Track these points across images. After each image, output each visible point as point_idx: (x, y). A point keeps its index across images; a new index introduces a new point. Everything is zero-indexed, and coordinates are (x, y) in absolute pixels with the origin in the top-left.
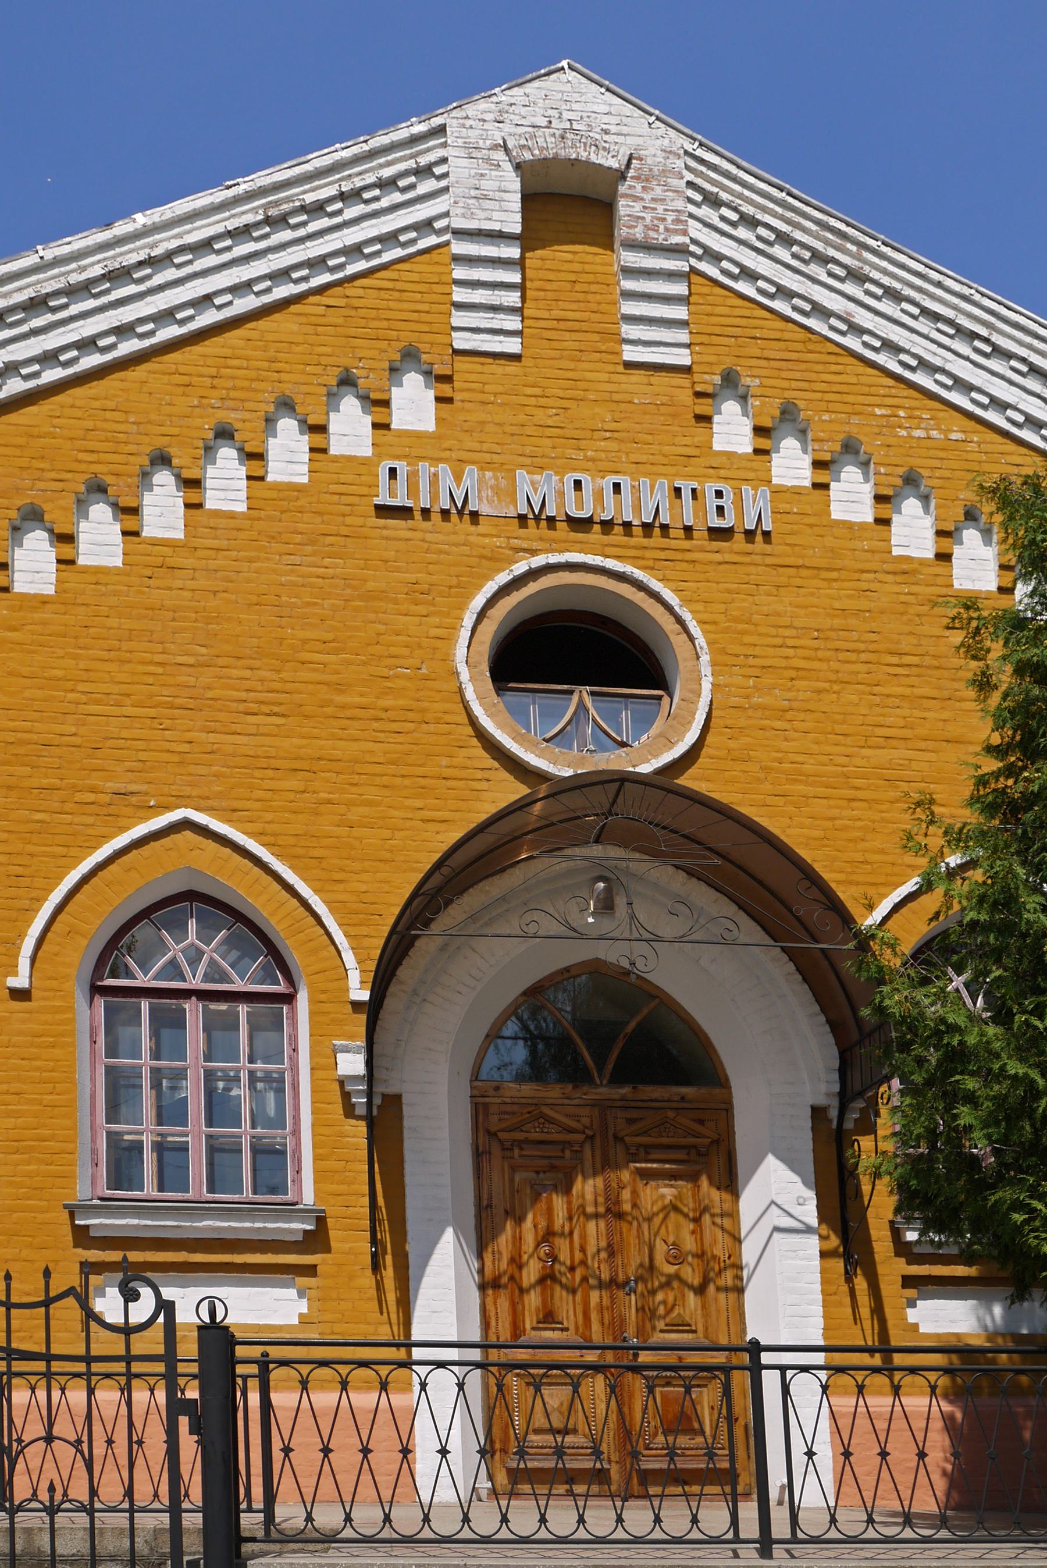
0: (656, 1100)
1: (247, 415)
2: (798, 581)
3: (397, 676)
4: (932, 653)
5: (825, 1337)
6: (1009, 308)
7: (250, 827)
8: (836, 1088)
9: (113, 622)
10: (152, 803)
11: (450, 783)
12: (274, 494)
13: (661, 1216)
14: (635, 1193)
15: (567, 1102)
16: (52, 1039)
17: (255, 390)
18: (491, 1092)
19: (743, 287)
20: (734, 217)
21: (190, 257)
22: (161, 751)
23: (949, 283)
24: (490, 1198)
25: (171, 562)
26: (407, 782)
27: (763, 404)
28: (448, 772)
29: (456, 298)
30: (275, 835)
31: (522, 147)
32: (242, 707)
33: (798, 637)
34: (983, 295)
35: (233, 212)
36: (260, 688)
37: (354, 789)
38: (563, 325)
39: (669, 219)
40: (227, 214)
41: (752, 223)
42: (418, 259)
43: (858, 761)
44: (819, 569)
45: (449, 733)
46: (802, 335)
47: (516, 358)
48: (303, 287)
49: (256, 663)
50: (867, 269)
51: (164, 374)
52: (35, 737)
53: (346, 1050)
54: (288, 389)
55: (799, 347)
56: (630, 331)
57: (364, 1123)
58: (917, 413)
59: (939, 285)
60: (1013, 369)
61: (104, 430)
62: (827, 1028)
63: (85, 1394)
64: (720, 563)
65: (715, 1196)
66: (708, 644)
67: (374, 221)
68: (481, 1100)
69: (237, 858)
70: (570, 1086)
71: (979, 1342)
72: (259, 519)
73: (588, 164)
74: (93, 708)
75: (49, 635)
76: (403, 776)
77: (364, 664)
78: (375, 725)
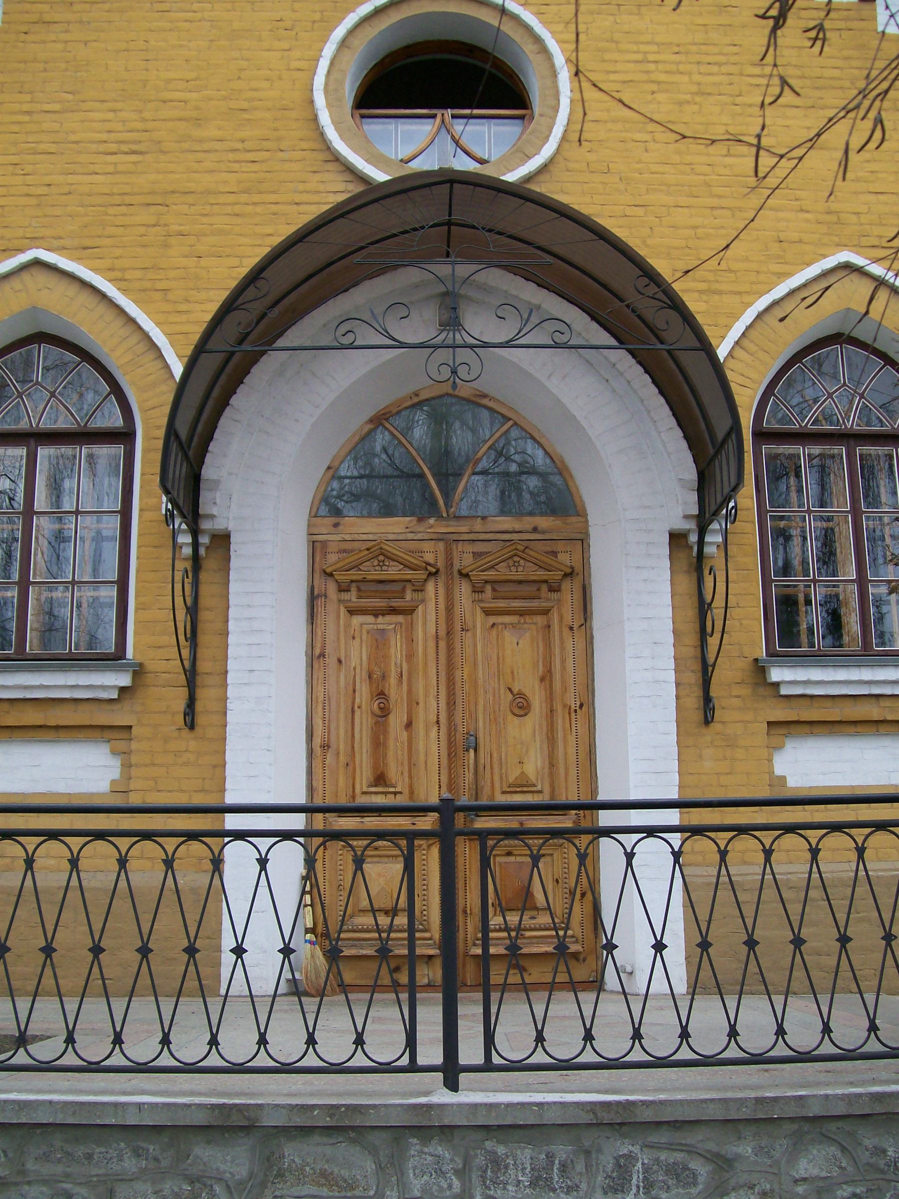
4: (794, 63)
7: (98, 263)
8: (695, 512)
15: (410, 536)
24: (324, 647)
25: (47, 18)
28: (298, 198)
30: (123, 270)
32: (102, 147)
33: (659, 53)
37: (205, 220)
49: (119, 105)
77: (225, 98)
78: (231, 156)
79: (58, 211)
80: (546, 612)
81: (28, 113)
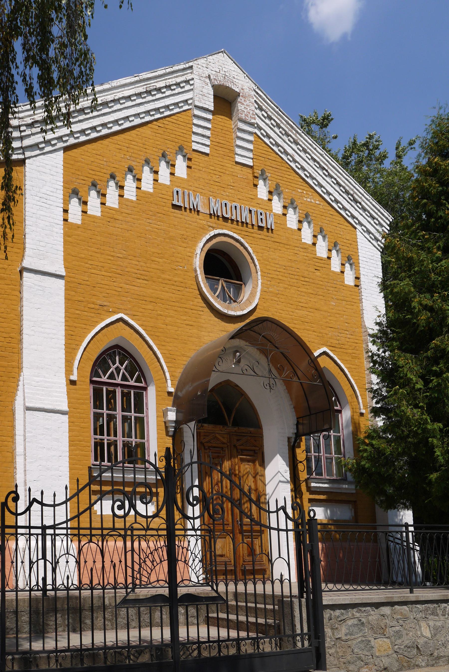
0: (243, 433)
2: (279, 248)
3: (179, 269)
6: (332, 161)
9: (99, 238)
10: (111, 310)
11: (194, 311)
12: (144, 195)
13: (246, 476)
14: (239, 467)
16: (83, 401)
17: (139, 155)
19: (266, 140)
20: (266, 115)
21: (124, 101)
22: (113, 290)
23: (318, 149)
25: (116, 217)
26: (181, 309)
29: (194, 130)
30: (146, 326)
31: (215, 79)
34: (326, 155)
35: (136, 86)
36: (141, 269)
37: (167, 311)
38: (219, 145)
39: (251, 113)
40: (134, 86)
41: (270, 118)
42: (182, 113)
43: (295, 314)
45: (192, 293)
46: (280, 160)
47: (207, 154)
48: (153, 118)
49: (140, 259)
50: (299, 141)
51: (114, 144)
52: (76, 280)
53: (171, 411)
54: (149, 156)
55: (279, 164)
56: (238, 151)
57: (171, 438)
58: (308, 193)
59: (315, 149)
60: (332, 182)
61: (97, 163)
63: (78, 543)
64: (261, 239)
65: (259, 468)
67: (173, 97)
69: (135, 334)
71: (325, 522)
72: (140, 204)
73: (231, 88)
74: (93, 271)
75: (80, 240)
76: (180, 307)
78: (173, 287)
79: (125, 299)
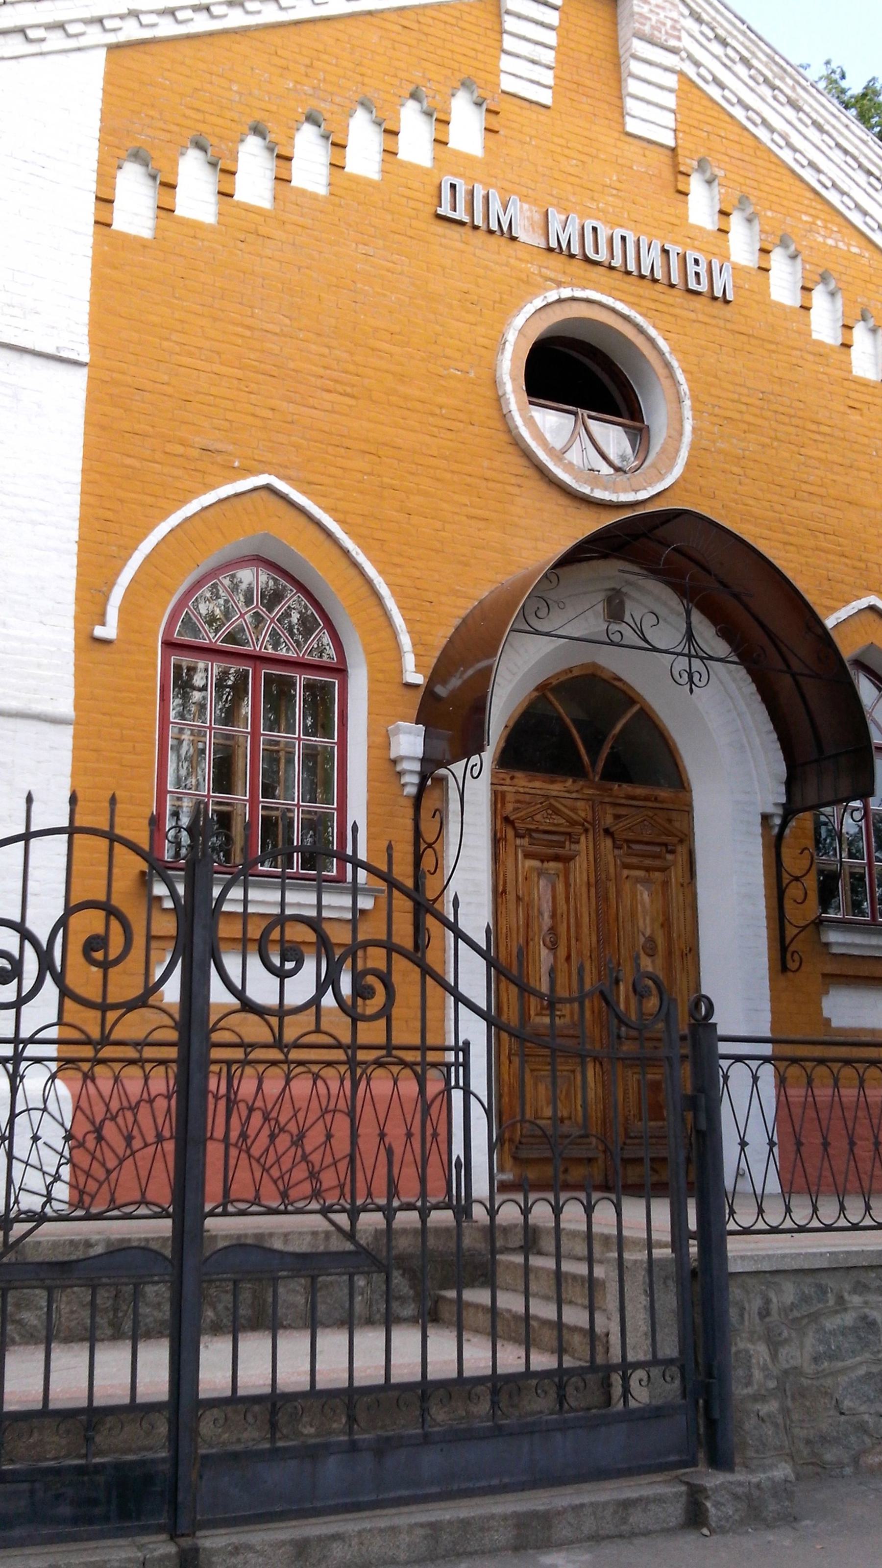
1: (335, 108)
5: (772, 1030)
8: (783, 800)
10: (236, 464)
11: (491, 485)
15: (567, 795)
18: (508, 781)
25: (262, 230)
27: (727, 193)
28: (489, 474)
32: (319, 382)
36: (336, 367)
44: (763, 340)
62: (778, 745)
66: (690, 390)
68: (500, 788)
70: (570, 781)
78: (431, 419)
80: (663, 870)
81: (249, 327)
